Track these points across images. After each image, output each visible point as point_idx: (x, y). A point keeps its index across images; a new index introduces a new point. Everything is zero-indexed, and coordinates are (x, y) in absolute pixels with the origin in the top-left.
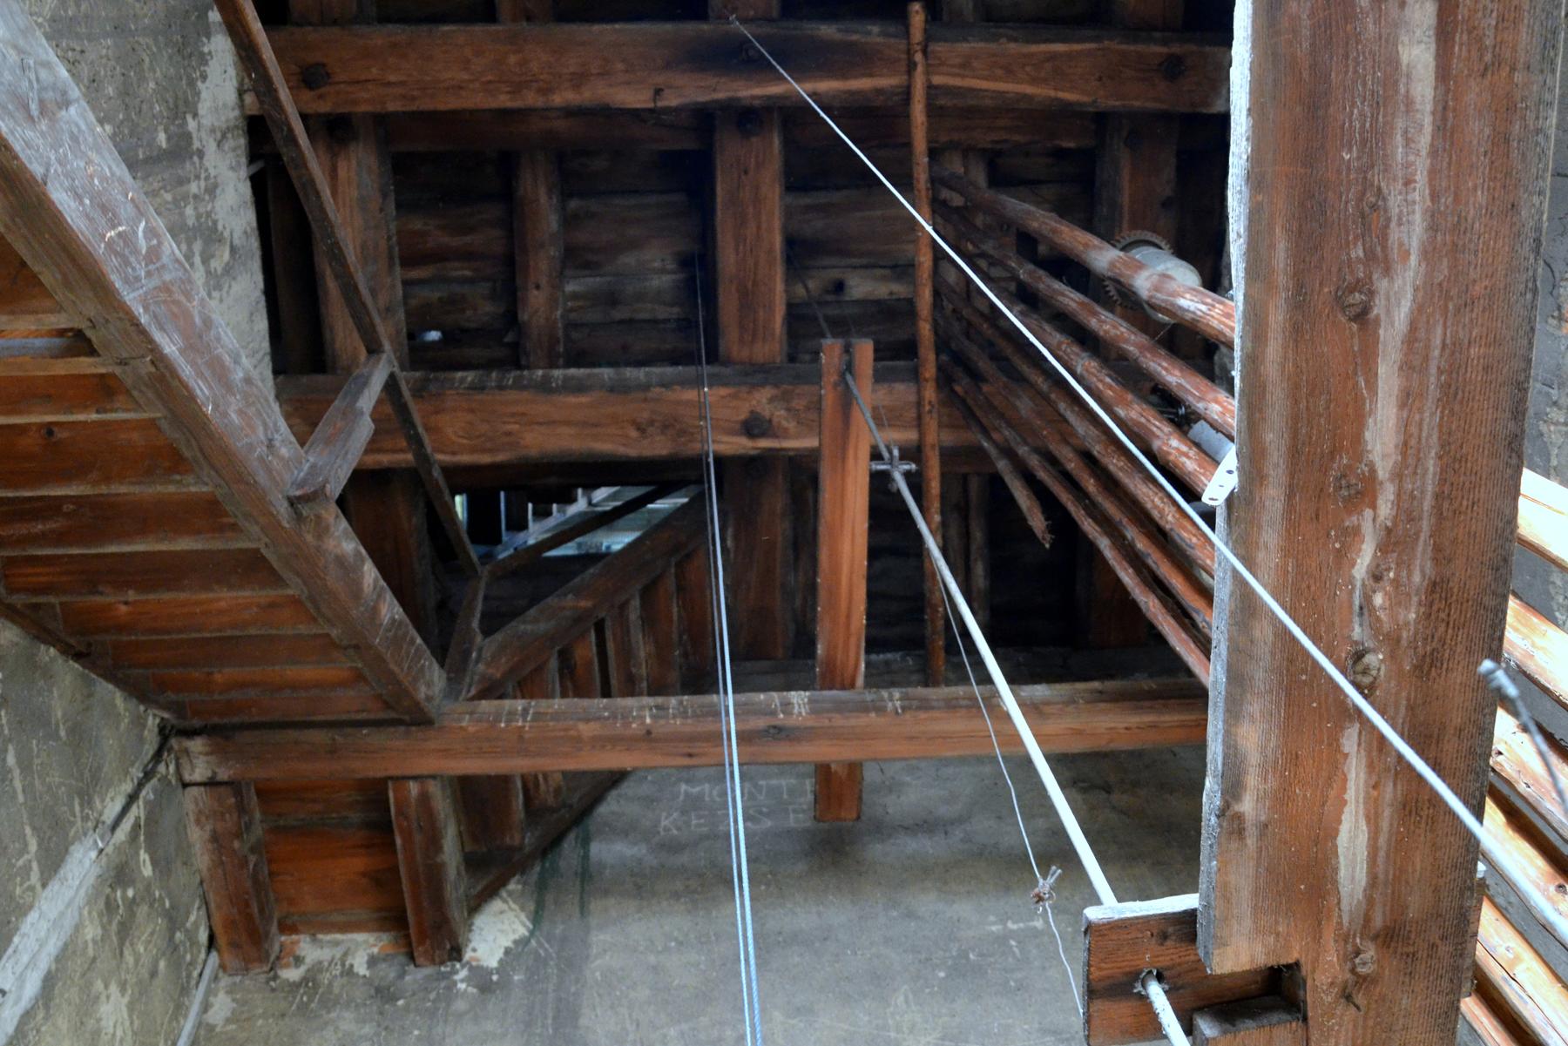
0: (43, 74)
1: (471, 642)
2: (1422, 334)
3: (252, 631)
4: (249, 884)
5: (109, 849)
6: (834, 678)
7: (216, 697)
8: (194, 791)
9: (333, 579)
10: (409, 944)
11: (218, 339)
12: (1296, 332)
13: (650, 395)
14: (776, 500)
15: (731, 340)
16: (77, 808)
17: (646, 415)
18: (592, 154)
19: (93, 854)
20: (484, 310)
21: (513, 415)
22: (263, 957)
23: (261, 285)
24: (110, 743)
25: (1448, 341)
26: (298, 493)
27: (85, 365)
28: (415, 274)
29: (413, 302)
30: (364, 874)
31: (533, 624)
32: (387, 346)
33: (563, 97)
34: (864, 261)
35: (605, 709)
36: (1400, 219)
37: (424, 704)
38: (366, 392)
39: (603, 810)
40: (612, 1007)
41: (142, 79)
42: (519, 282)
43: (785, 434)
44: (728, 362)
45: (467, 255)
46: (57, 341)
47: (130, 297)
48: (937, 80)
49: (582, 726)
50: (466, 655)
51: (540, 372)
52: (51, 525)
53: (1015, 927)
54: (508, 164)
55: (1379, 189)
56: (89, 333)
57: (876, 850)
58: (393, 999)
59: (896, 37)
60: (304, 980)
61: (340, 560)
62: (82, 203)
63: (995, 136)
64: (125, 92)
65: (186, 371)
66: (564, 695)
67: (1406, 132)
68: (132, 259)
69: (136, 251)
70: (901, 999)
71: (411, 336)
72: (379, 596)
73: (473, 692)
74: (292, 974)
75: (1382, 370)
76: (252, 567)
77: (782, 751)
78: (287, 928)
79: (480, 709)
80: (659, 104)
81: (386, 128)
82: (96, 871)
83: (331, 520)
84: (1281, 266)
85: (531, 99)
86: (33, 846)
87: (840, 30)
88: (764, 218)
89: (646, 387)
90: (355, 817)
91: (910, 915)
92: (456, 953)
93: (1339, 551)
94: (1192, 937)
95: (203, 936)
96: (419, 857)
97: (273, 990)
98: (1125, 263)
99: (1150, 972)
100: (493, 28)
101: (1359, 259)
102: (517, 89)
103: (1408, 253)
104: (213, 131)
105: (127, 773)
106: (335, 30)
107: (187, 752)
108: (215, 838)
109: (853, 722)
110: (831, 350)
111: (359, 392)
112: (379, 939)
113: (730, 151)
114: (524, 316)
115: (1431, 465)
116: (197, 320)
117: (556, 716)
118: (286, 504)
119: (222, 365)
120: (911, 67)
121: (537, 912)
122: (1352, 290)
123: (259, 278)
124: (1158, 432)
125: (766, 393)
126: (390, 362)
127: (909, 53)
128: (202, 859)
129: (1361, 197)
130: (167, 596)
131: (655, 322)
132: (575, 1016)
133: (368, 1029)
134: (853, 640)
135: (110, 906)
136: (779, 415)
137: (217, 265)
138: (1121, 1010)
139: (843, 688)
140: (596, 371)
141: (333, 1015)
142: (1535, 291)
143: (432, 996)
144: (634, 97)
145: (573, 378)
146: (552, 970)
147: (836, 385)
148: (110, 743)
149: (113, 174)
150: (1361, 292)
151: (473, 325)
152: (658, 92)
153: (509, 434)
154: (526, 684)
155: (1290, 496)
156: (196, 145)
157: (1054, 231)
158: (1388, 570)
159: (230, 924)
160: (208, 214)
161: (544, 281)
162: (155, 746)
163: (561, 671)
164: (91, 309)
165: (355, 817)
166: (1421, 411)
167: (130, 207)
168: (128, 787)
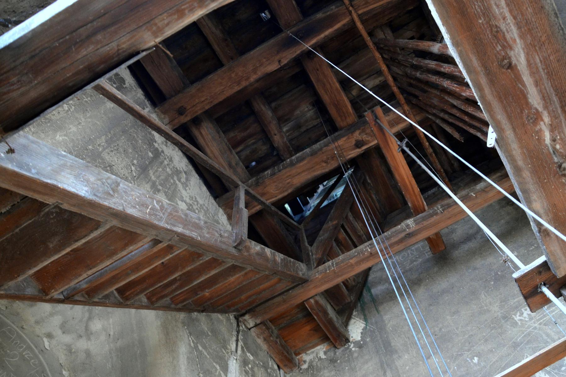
0: (109, 181)
1: (308, 250)
2: (532, 61)
3: (244, 283)
4: (280, 348)
5: (238, 358)
6: (418, 211)
7: (245, 303)
8: (253, 329)
9: (259, 261)
10: (333, 344)
11: (191, 217)
12: (492, 82)
13: (323, 151)
14: (376, 162)
15: (340, 123)
16: (224, 351)
17: (325, 157)
18: (271, 89)
19: (235, 361)
20: (263, 149)
21: (287, 177)
22: (295, 365)
23: (198, 177)
24: (223, 329)
25: (542, 59)
26: (236, 244)
27: (161, 246)
28: (239, 149)
29: (242, 157)
30: (310, 330)
31: (323, 236)
32: (240, 183)
33: (253, 78)
34: (367, 76)
35: (355, 252)
36: (507, 31)
37: (304, 277)
38: (241, 201)
39: (370, 278)
40: (399, 336)
41: (137, 141)
42: (269, 136)
43: (369, 142)
44: (341, 129)
45: (250, 136)
46: (150, 243)
47: (162, 224)
48: (360, 12)
49: (351, 261)
50: (308, 254)
51: (288, 160)
52: (176, 285)
54: (248, 104)
55: (496, 26)
56: (157, 238)
57: (456, 253)
58: (336, 361)
59: (341, 6)
60: (309, 366)
61: (258, 254)
62: (136, 208)
63: (386, 18)
64: (134, 148)
65: (187, 232)
66: (343, 253)
67: (496, 4)
68: (157, 213)
69: (157, 210)
70: (483, 296)
71: (247, 167)
72: (274, 256)
73: (315, 265)
74: (305, 366)
75: (525, 79)
76: (234, 269)
77: (413, 240)
78: (297, 354)
79: (320, 270)
80: (282, 65)
81: (209, 114)
82: (238, 365)
83: (249, 244)
84: (477, 65)
85: (244, 84)
86: (218, 367)
87: (323, 13)
88: (330, 81)
89: (321, 149)
90: (300, 315)
91: (475, 269)
92: (347, 340)
93: (538, 139)
94: (549, 269)
95: (276, 367)
96: (323, 319)
97: (302, 373)
98: (443, 48)
99: (541, 284)
100: (223, 69)
101: (500, 50)
102: (239, 83)
103: (515, 40)
104: (163, 143)
105: (232, 335)
106: (180, 95)
107: (245, 320)
108: (265, 339)
109: (429, 222)
110: (368, 115)
111: (238, 204)
112: (324, 346)
113: (309, 66)
114: (276, 145)
115: (555, 99)
116: (183, 216)
117: (342, 261)
118: (234, 249)
119: (197, 224)
120: (350, 13)
121: (365, 318)
122: (503, 60)
123: (197, 176)
125: (357, 133)
126: (243, 187)
127: (347, 9)
128: (265, 347)
129: (491, 31)
130: (218, 286)
131: (315, 126)
132: (389, 343)
133: (333, 373)
134: (418, 197)
135: (246, 372)
136: (364, 137)
137: (183, 180)
138: (537, 298)
139: (422, 212)
140: (304, 151)
141: (322, 373)
142: (562, 29)
143: (347, 355)
144: (274, 67)
145: (299, 157)
146: (377, 333)
147: (375, 125)
148: (223, 329)
149: (140, 194)
150: (506, 59)
151: (263, 155)
152: (279, 61)
153: (289, 183)
154: (329, 255)
155: (514, 131)
156: (160, 150)
157: (417, 46)
158: (557, 136)
159: (281, 360)
160: (174, 167)
161: (276, 132)
162: (236, 323)
163: (338, 245)
164: (154, 232)
165: (300, 315)
166: (543, 84)
167: (149, 199)
168: (234, 338)
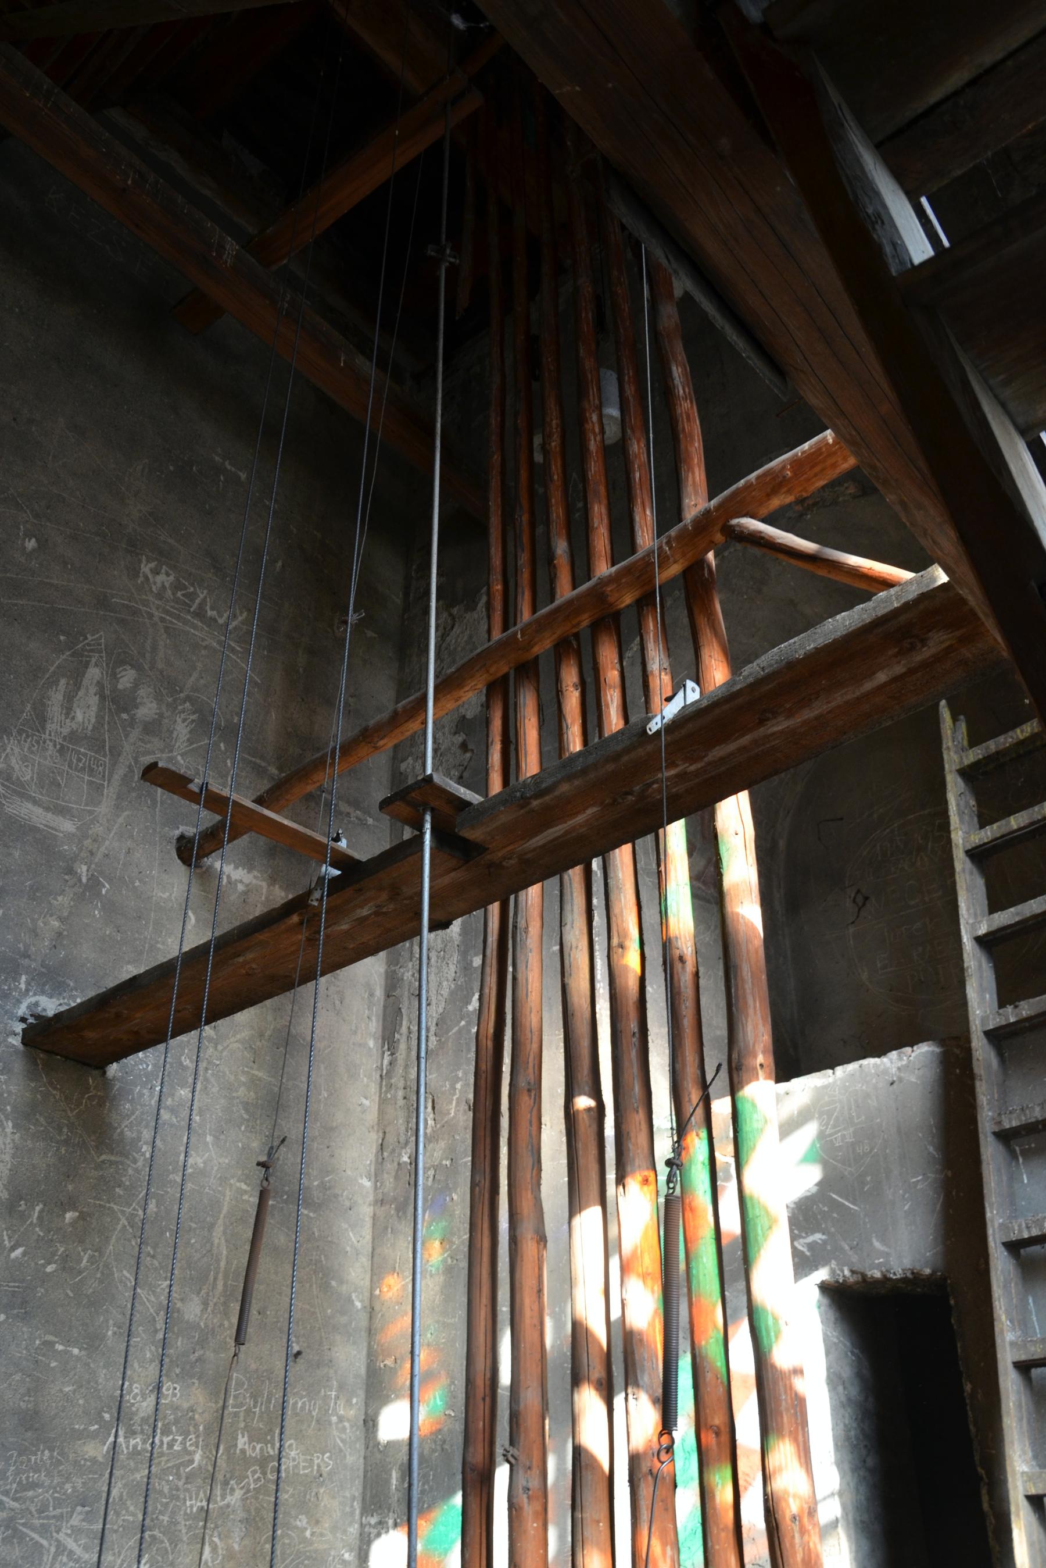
53: (229, 467)
124: (591, 398)
